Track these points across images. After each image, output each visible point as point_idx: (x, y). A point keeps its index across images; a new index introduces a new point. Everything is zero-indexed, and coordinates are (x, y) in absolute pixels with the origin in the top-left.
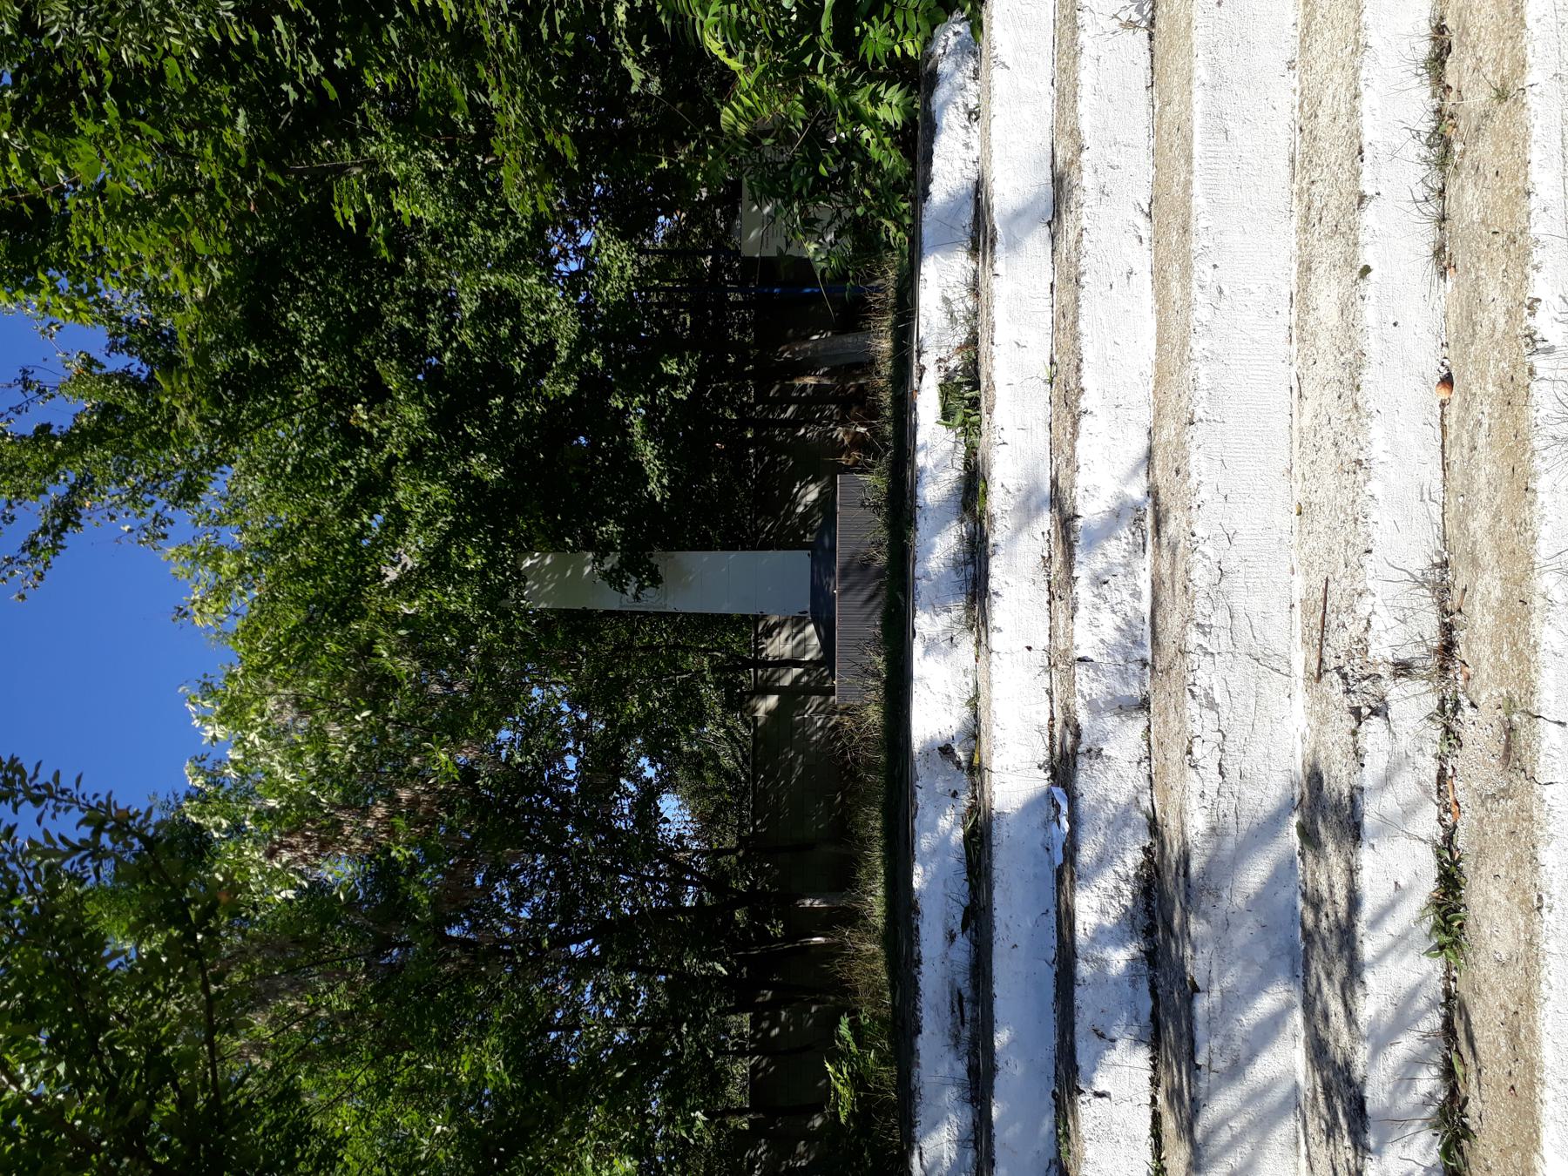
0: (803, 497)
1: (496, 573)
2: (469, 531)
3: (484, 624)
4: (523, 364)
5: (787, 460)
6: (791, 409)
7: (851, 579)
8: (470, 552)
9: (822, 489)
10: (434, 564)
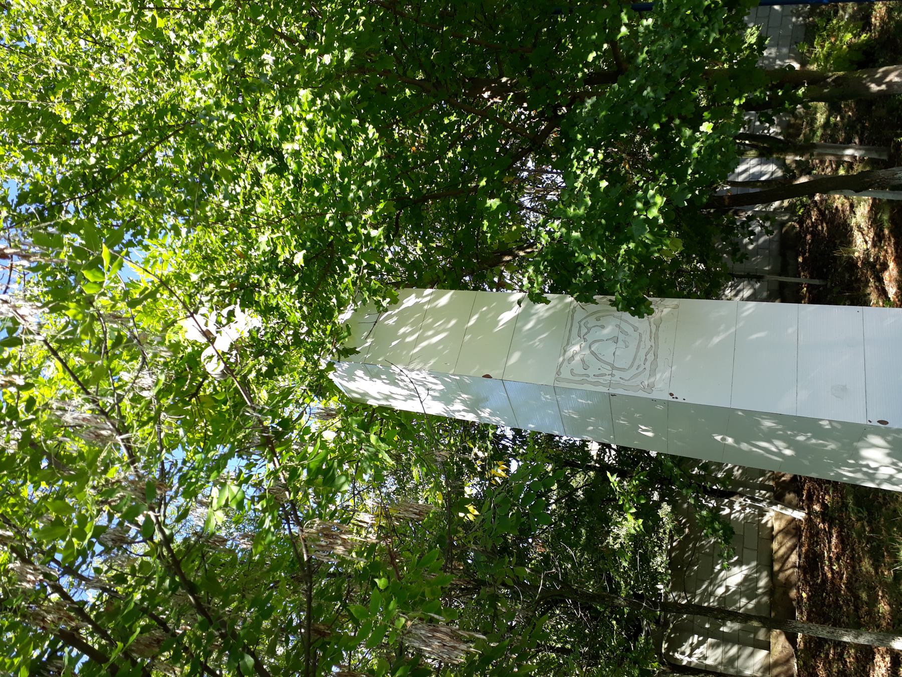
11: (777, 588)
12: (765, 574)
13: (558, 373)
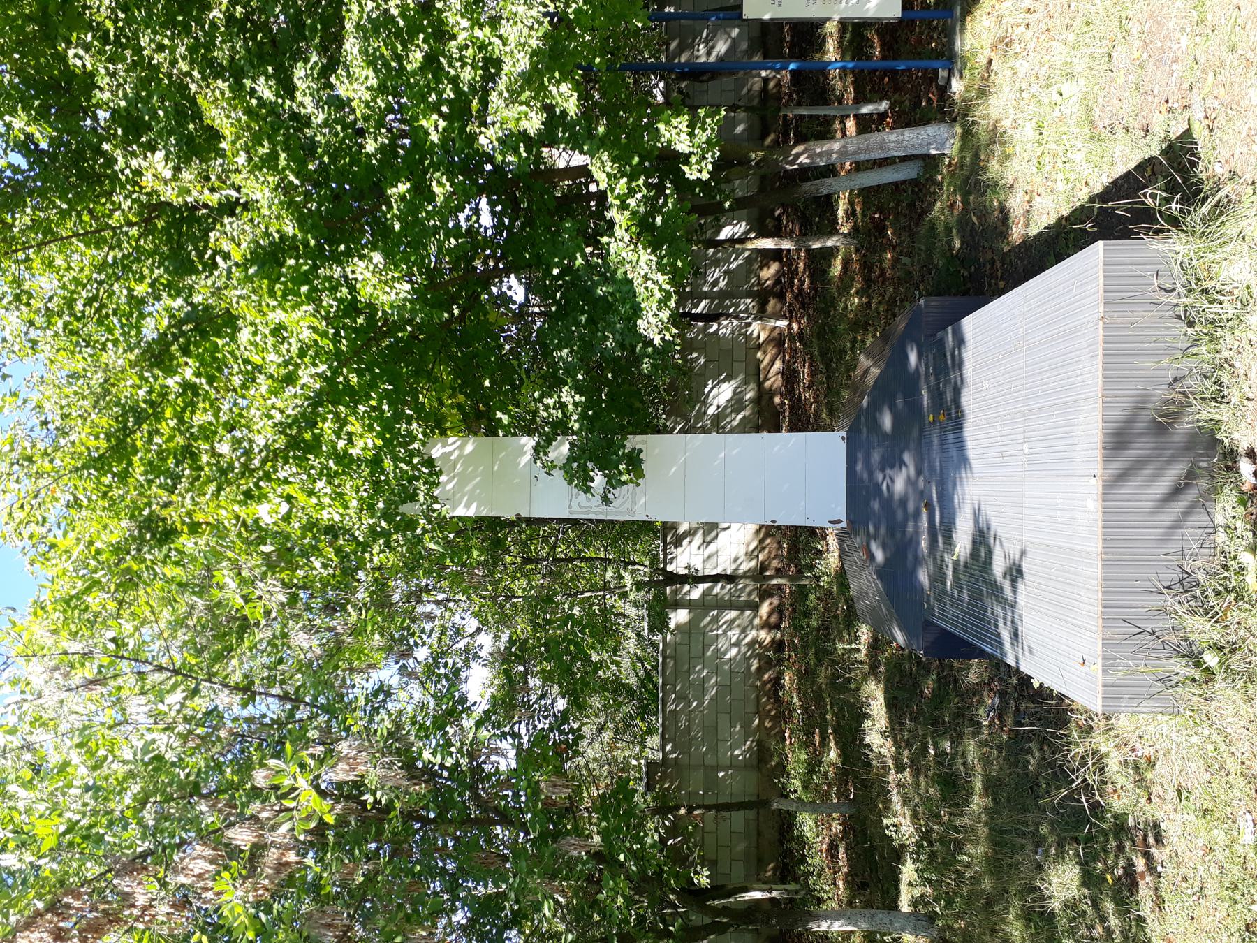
0: (714, 398)
1: (395, 459)
2: (355, 396)
3: (374, 541)
4: (442, 124)
5: (698, 358)
6: (704, 303)
7: (1133, 453)
8: (355, 427)
9: (736, 388)
10: (294, 443)
11: (764, 397)
12: (752, 386)
13: (570, 507)
